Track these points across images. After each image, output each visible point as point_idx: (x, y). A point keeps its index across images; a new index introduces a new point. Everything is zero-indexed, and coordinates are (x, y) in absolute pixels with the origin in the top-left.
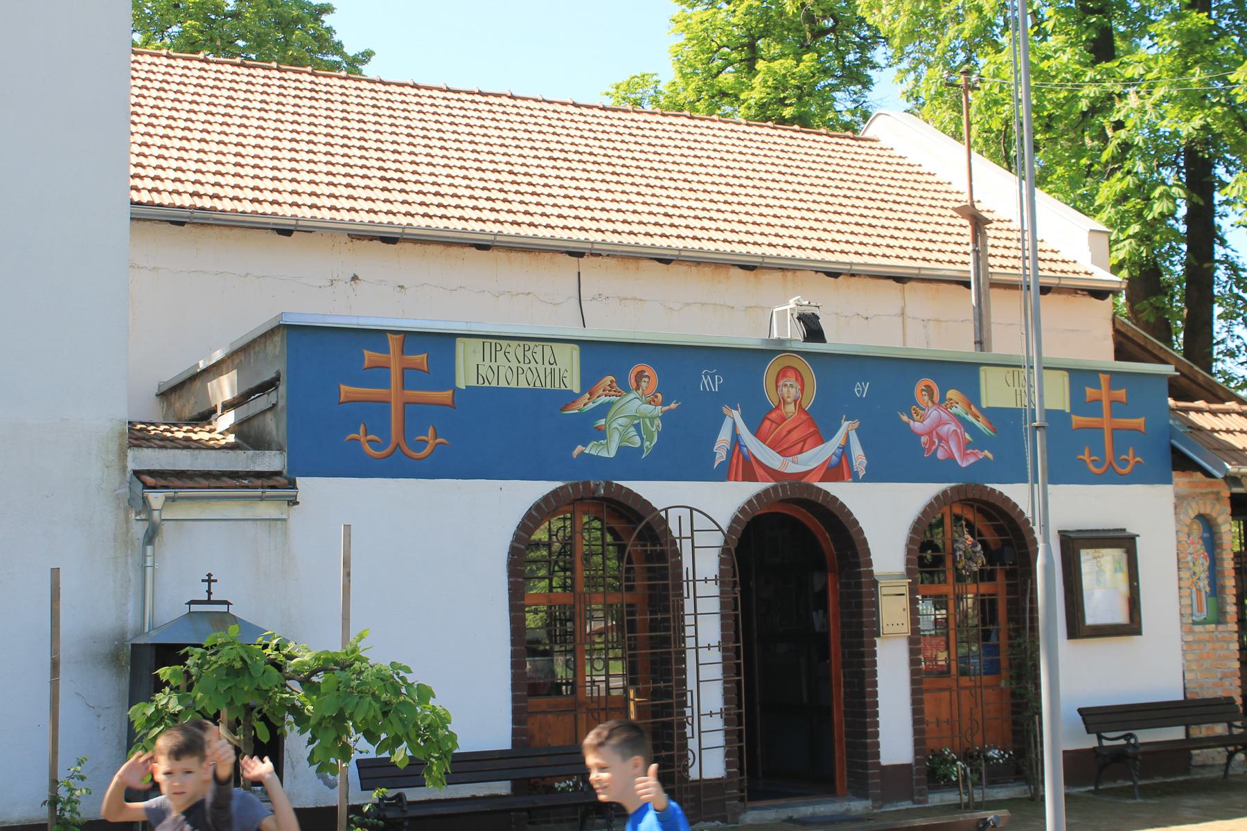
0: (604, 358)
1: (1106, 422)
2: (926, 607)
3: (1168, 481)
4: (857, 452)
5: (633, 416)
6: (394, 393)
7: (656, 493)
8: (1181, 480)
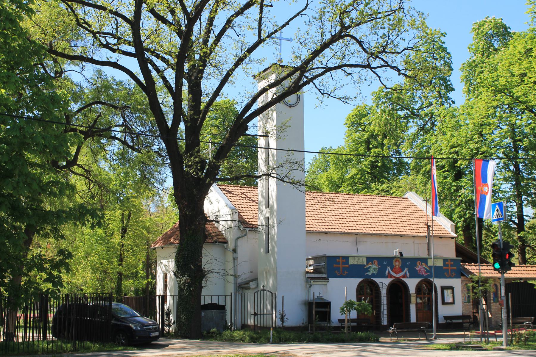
0: (370, 259)
1: (449, 268)
2: (418, 299)
3: (460, 278)
4: (408, 273)
5: (374, 268)
6: (341, 266)
7: (377, 280)
8: (462, 278)
